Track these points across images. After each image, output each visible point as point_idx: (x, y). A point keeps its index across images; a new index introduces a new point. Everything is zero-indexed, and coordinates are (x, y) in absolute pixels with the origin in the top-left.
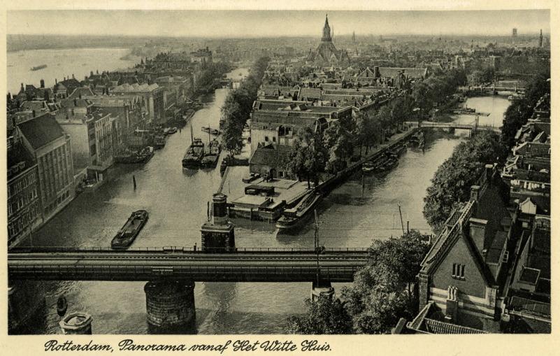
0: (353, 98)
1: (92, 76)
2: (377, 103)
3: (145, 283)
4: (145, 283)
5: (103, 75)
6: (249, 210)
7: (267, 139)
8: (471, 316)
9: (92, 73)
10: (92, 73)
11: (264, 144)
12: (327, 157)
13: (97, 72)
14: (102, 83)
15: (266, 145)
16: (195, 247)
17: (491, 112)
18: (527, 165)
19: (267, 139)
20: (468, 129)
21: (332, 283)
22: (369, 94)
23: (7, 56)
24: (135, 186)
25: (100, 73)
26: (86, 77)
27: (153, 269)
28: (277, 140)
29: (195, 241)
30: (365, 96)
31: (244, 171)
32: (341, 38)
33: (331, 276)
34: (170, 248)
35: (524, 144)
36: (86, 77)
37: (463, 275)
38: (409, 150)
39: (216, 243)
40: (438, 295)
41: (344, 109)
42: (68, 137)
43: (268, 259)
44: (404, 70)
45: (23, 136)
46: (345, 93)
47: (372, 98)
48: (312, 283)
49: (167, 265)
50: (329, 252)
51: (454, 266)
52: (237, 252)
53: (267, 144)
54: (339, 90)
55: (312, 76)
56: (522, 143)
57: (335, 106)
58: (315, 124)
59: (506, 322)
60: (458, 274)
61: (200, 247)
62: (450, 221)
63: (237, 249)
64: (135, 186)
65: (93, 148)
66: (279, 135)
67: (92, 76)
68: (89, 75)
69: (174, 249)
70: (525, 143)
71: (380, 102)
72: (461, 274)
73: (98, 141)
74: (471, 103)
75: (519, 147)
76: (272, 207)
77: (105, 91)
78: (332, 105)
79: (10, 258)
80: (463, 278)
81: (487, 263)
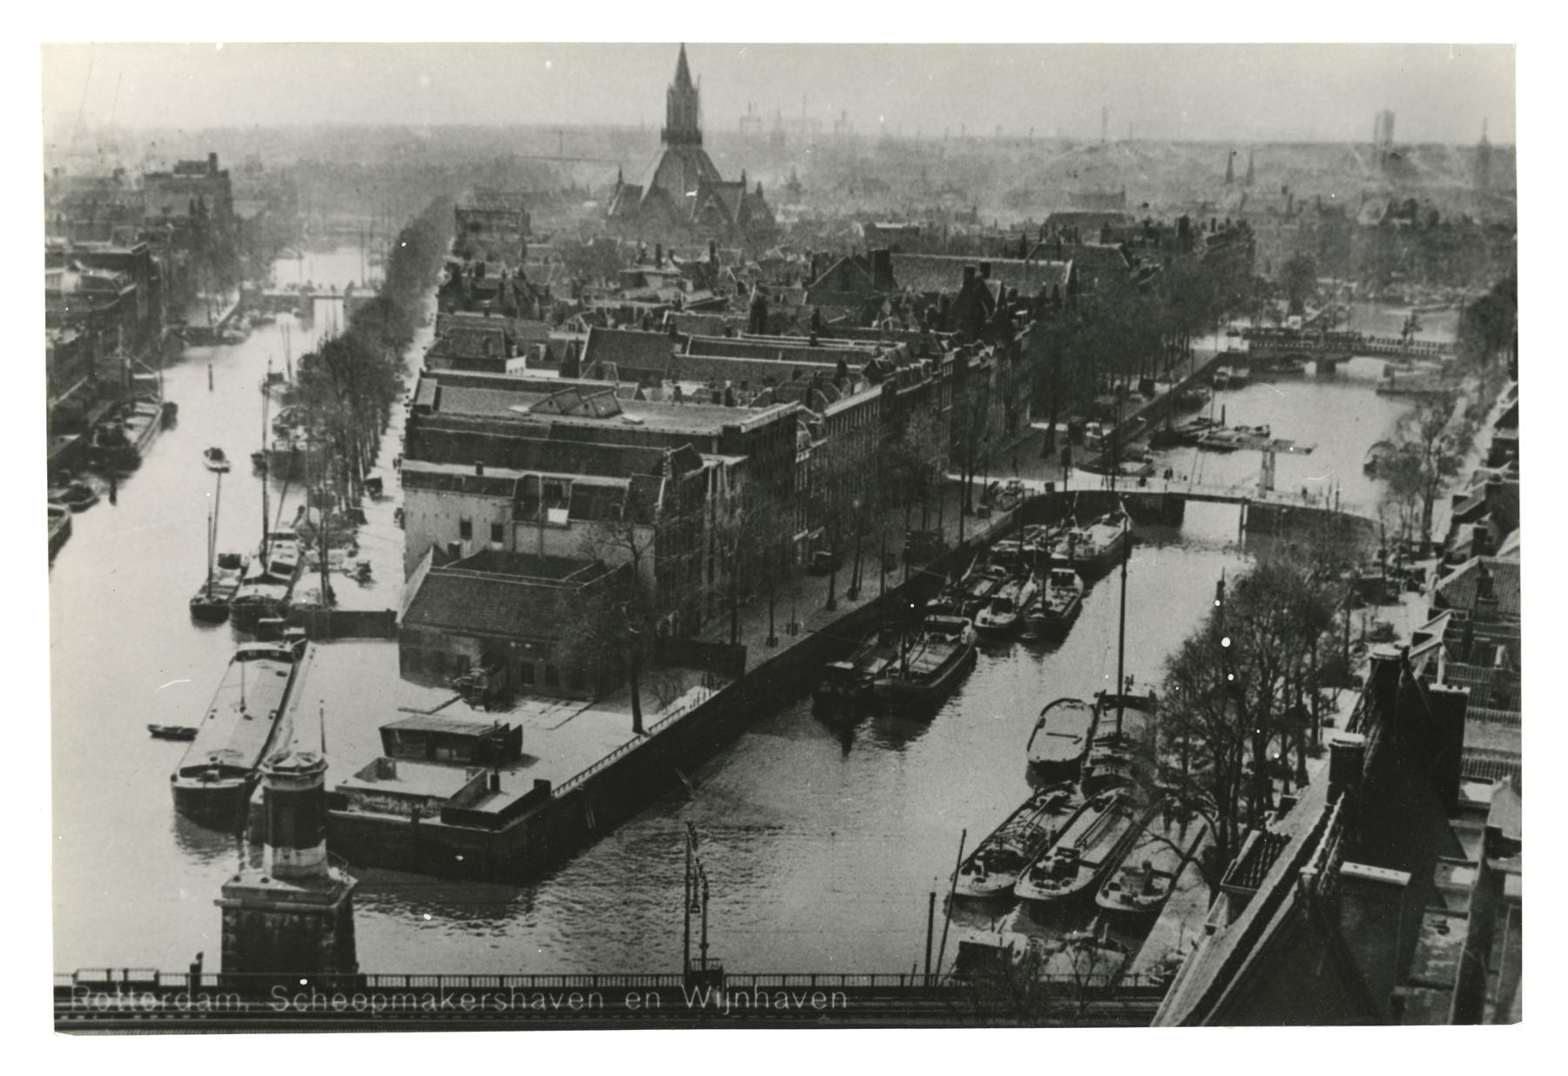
7: (466, 529)
11: (455, 550)
12: (927, 365)
19: (466, 529)
20: (1233, 501)
24: (1105, 121)
30: (842, 366)
34: (102, 977)
38: (983, 660)
44: (986, 268)
46: (770, 352)
53: (468, 549)
54: (740, 337)
58: (658, 471)
59: (1432, 881)
63: (363, 977)
64: (1105, 121)
66: (515, 516)
69: (117, 977)
70: (1474, 561)
74: (1236, 408)
76: (494, 806)
81: (1284, 325)
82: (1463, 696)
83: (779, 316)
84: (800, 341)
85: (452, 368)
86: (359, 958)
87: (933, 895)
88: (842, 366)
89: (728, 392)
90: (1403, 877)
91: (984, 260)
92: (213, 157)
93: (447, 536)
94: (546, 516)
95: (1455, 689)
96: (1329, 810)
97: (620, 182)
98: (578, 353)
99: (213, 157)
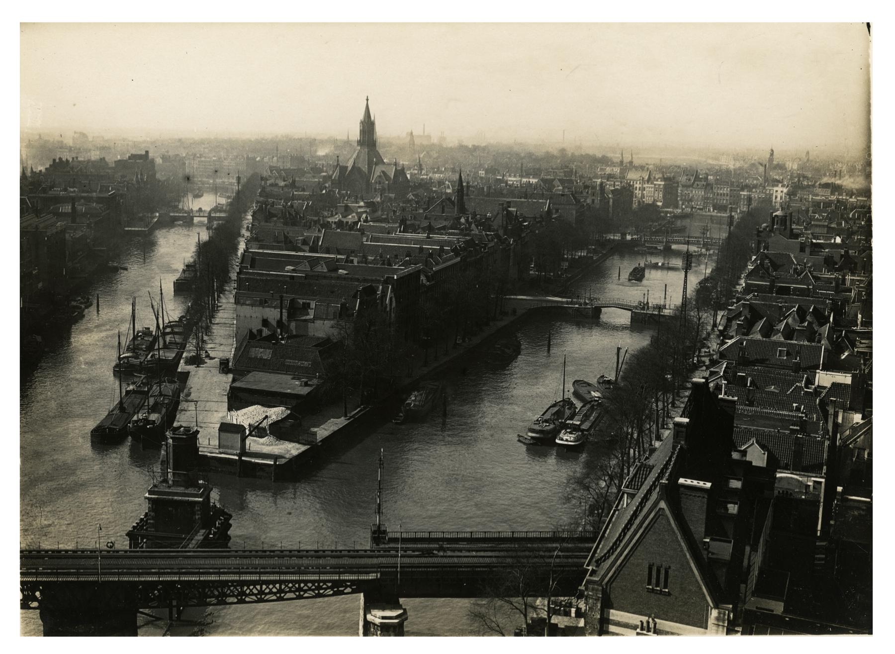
0: (421, 249)
11: (260, 331)
15: (264, 335)
18: (744, 379)
21: (401, 600)
22: (449, 243)
23: (22, 614)
30: (442, 247)
35: (733, 340)
41: (406, 270)
42: (723, 154)
44: (509, 202)
45: (532, 391)
50: (395, 540)
51: (650, 569)
53: (266, 332)
55: (343, 210)
56: (731, 338)
57: (390, 264)
58: (355, 297)
60: (657, 585)
70: (738, 338)
72: (654, 581)
82: (734, 402)
83: (413, 225)
84: (422, 236)
85: (259, 249)
86: (91, 541)
87: (619, 349)
88: (442, 247)
89: (389, 260)
90: (682, 481)
91: (508, 200)
92: (147, 152)
93: (256, 326)
94: (112, 168)
95: (730, 398)
96: (673, 453)
97: (338, 165)
98: (318, 242)
99: (147, 152)
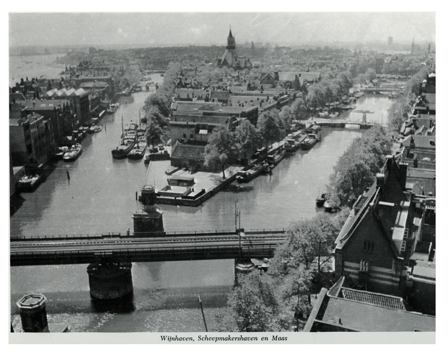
1: (22, 83)
2: (278, 103)
3: (87, 265)
4: (87, 265)
5: (33, 82)
6: (173, 198)
7: (185, 136)
8: (380, 284)
9: (22, 80)
10: (22, 80)
13: (27, 79)
14: (32, 89)
16: (128, 232)
17: (378, 110)
22: (272, 95)
25: (30, 79)
26: (17, 84)
27: (94, 253)
28: (194, 136)
29: (129, 226)
31: (166, 165)
32: (241, 47)
33: (251, 253)
36: (17, 84)
37: (373, 250)
39: (148, 226)
40: (350, 268)
43: (217, 240)
46: (252, 95)
47: (275, 99)
48: (234, 260)
49: (107, 248)
51: (365, 243)
52: (164, 235)
61: (132, 233)
62: (357, 204)
63: (165, 233)
65: (29, 147)
67: (22, 83)
68: (19, 82)
69: (111, 234)
71: (281, 103)
73: (33, 141)
75: (404, 140)
77: (36, 96)
78: (240, 105)
79: (12, 247)
80: (373, 252)
